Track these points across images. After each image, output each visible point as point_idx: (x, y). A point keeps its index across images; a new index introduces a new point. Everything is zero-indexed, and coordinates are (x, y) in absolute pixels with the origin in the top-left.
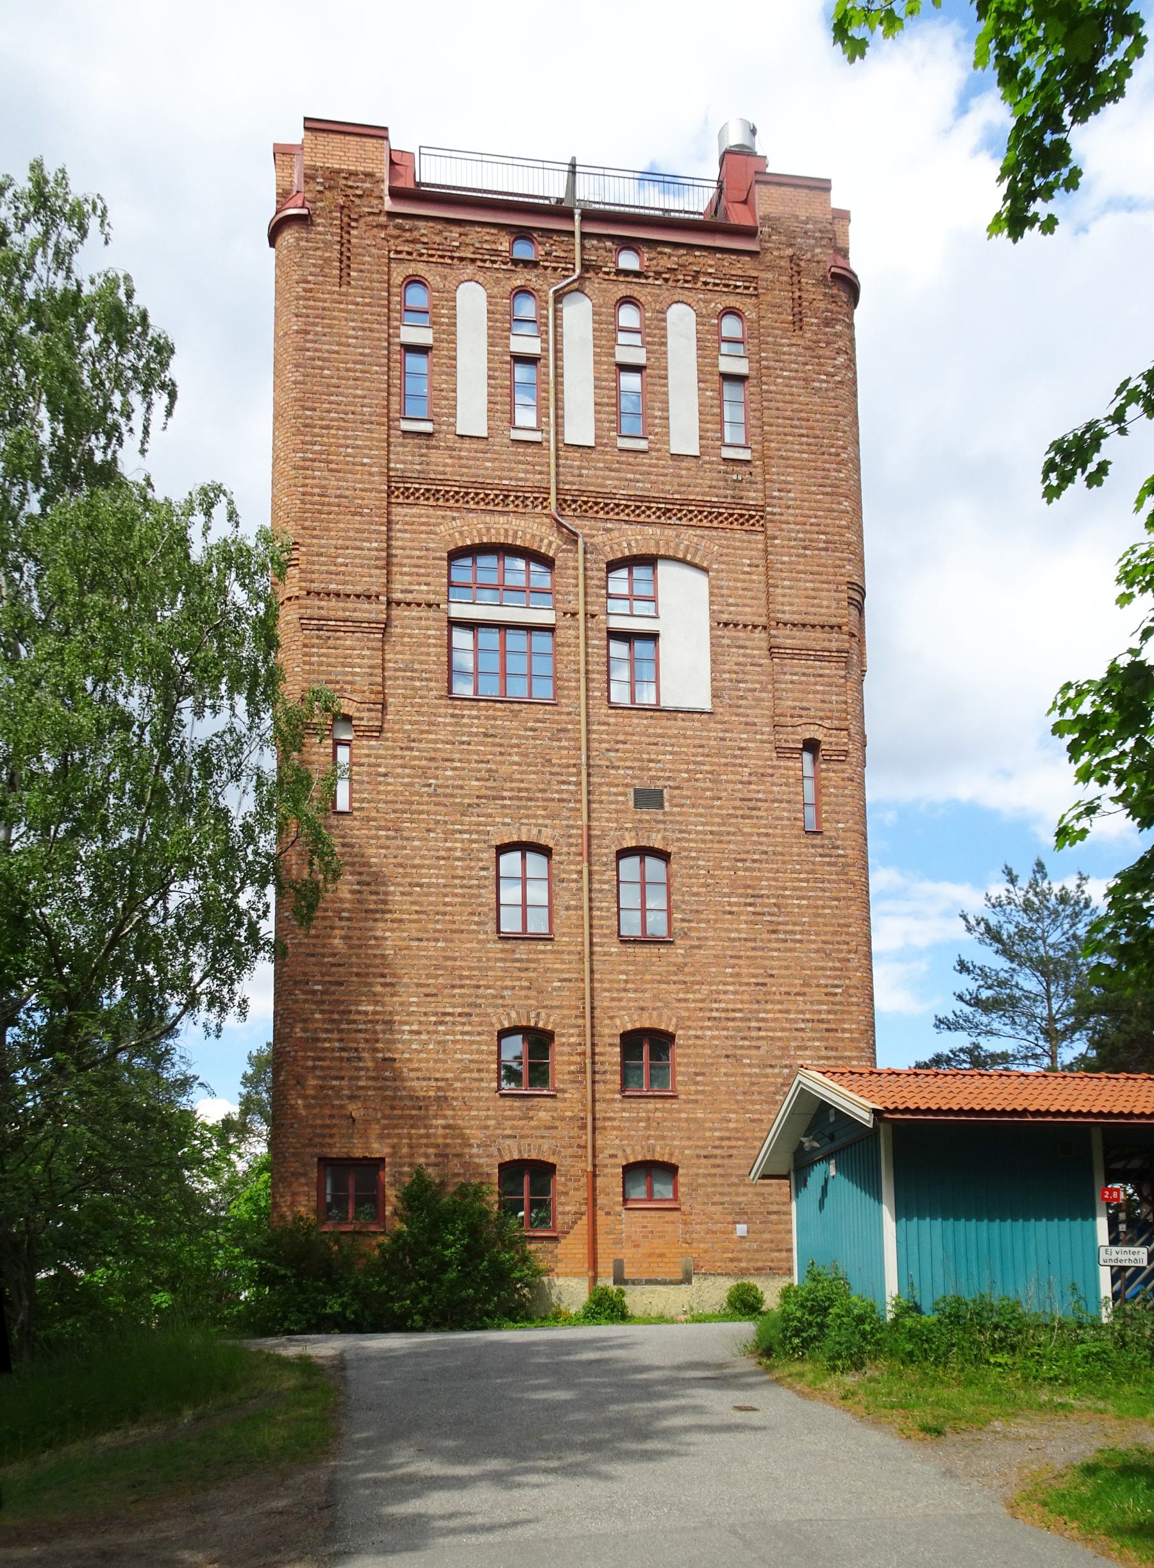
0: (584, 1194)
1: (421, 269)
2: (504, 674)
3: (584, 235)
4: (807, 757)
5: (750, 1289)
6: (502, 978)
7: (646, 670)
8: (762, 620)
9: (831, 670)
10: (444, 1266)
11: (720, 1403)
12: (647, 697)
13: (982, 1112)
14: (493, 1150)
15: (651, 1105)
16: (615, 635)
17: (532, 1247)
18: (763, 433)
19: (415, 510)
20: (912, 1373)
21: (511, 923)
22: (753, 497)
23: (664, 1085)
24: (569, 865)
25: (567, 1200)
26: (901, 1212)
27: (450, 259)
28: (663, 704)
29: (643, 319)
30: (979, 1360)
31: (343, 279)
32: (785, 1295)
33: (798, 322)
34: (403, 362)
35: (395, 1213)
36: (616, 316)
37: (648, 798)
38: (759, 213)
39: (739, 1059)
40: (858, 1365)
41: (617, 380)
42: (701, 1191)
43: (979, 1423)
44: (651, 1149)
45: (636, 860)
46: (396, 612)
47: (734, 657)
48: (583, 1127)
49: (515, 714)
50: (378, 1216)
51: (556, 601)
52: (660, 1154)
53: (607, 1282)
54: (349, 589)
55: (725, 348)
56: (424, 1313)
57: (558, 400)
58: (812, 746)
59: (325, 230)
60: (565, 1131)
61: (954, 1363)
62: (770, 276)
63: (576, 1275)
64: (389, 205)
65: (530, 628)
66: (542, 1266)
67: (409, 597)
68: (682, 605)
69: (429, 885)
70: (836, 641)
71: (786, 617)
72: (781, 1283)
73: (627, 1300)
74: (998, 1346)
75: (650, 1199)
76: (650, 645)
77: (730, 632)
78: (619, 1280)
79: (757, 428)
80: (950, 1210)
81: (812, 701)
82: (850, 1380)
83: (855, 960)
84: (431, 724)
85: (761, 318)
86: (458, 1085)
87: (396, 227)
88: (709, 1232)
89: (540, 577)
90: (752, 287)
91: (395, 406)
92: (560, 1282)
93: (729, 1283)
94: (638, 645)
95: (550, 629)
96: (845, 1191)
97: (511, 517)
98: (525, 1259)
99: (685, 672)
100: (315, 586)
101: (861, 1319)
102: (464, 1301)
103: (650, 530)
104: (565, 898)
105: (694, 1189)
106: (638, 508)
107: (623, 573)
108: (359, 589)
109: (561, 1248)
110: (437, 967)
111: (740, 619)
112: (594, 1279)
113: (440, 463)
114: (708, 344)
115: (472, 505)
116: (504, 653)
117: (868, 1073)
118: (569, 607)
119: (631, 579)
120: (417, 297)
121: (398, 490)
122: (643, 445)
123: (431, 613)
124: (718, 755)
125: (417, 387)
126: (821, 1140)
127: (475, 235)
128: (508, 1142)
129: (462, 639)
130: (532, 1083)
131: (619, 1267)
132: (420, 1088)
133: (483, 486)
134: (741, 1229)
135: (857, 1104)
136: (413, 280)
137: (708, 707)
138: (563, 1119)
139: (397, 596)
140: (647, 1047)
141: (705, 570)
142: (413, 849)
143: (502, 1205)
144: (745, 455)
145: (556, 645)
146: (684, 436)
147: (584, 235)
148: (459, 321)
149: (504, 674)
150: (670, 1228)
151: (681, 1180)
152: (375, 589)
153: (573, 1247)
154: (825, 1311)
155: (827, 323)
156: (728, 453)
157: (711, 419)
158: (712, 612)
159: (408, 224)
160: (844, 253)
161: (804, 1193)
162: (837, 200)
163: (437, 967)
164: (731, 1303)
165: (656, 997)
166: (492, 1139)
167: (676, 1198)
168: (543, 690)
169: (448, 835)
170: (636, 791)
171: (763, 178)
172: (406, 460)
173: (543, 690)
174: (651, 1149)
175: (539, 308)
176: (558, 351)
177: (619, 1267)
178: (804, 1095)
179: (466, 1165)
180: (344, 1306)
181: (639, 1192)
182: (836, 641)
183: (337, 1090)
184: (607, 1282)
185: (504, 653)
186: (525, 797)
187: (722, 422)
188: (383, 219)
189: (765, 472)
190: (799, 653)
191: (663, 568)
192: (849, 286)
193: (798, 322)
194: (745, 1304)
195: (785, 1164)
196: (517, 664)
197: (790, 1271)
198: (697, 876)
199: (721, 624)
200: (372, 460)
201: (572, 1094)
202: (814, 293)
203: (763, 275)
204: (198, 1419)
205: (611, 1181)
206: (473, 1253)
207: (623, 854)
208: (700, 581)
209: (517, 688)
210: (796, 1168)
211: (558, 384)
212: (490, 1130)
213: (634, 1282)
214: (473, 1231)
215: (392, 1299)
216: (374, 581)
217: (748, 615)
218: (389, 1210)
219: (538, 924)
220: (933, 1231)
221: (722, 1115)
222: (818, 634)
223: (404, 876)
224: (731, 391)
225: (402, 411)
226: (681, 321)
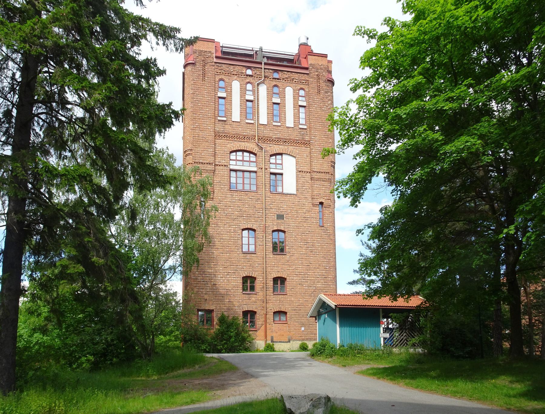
0: (263, 319)
1: (223, 77)
2: (243, 184)
3: (265, 69)
4: (320, 206)
5: (305, 344)
6: (243, 263)
7: (279, 183)
8: (309, 171)
9: (326, 184)
10: (231, 337)
11: (306, 363)
12: (280, 190)
13: (357, 305)
14: (241, 308)
15: (281, 296)
16: (271, 174)
17: (250, 333)
18: (310, 121)
19: (221, 141)
20: (342, 358)
21: (245, 249)
22: (307, 138)
23: (284, 292)
24: (259, 234)
25: (259, 320)
26: (341, 326)
27: (230, 74)
28: (285, 192)
29: (279, 91)
30: (355, 356)
31: (203, 80)
32: (314, 345)
33: (319, 92)
34: (218, 102)
35: (216, 324)
36: (272, 90)
37: (280, 217)
38: (309, 63)
39: (302, 285)
40: (331, 357)
41: (273, 107)
42: (293, 319)
43: (353, 365)
44: (280, 308)
45: (277, 233)
46: (217, 167)
47: (302, 180)
48: (264, 302)
49: (247, 195)
50: (212, 325)
51: (257, 165)
52: (283, 309)
53: (269, 342)
54: (205, 162)
55: (300, 98)
56: (225, 349)
57: (258, 112)
58: (321, 203)
59: (199, 66)
60: (259, 303)
61: (350, 355)
62: (312, 80)
63: (261, 340)
64: (215, 60)
65: (250, 172)
66: (254, 337)
67: (220, 164)
68: (288, 166)
69: (225, 239)
70: (328, 176)
71: (315, 170)
72: (314, 342)
73: (275, 346)
74: (358, 353)
75: (280, 321)
76: (281, 176)
77: (301, 173)
78: (272, 341)
79: (308, 118)
80: (351, 325)
81: (322, 192)
82: (330, 360)
83: (332, 259)
84: (225, 197)
85: (309, 91)
86: (232, 291)
87: (217, 66)
88: (295, 329)
89: (253, 158)
90: (307, 83)
91: (216, 113)
92: (257, 342)
93: (300, 342)
94: (278, 176)
95: (256, 172)
96: (329, 321)
97: (246, 143)
98: (249, 336)
99: (289, 184)
100: (196, 161)
101: (332, 348)
102: (235, 346)
103: (281, 146)
104: (259, 243)
105: (291, 318)
106: (278, 141)
107: (274, 157)
108: (207, 162)
109: (258, 333)
110: (227, 260)
111: (304, 170)
112: (266, 341)
113: (228, 128)
114: (296, 97)
115: (236, 139)
116: (243, 178)
117: (334, 294)
118: (260, 167)
119: (276, 159)
120: (222, 84)
121: (217, 135)
122: (279, 124)
123: (226, 168)
124: (298, 206)
125: (222, 108)
126: (323, 309)
127: (237, 68)
128: (245, 306)
129: (233, 174)
130: (250, 291)
131: (272, 338)
132: (222, 291)
133: (239, 134)
134: (303, 329)
135: (332, 303)
136: (221, 80)
137: (295, 193)
138: (258, 300)
139: (217, 163)
140: (279, 281)
141: (295, 157)
142: (221, 229)
143: (243, 322)
144: (305, 127)
145: (257, 176)
146: (290, 122)
147: (265, 69)
148: (233, 91)
149: (243, 184)
150: (285, 328)
151: (288, 316)
152: (211, 162)
153: (260, 333)
154: (325, 347)
155: (326, 92)
156: (301, 126)
157: (297, 116)
158: (297, 168)
159: (220, 65)
160: (330, 72)
161: (320, 321)
162: (329, 58)
163: (227, 260)
164: (300, 348)
165: (282, 269)
166: (241, 305)
167: (286, 321)
168: (254, 188)
169: (230, 226)
170: (277, 215)
171: (311, 53)
172: (219, 127)
173: (254, 188)
174: (280, 308)
175: (253, 87)
176: (258, 99)
177: (272, 338)
178: (320, 300)
179: (234, 312)
180: (206, 347)
181: (277, 319)
182: (328, 176)
183: (202, 292)
184: (269, 342)
185: (243, 178)
186: (249, 216)
187: (299, 118)
188: (213, 64)
189: (310, 132)
190: (319, 179)
191: (284, 156)
192: (332, 82)
193: (319, 92)
194: (304, 348)
195: (316, 314)
196: (247, 181)
197: (315, 339)
198: (292, 237)
199: (299, 171)
200: (210, 127)
201: (261, 294)
202: (323, 85)
203: (310, 80)
204: (200, 367)
205: (270, 316)
206: (238, 334)
207: (273, 231)
208: (293, 160)
209: (247, 187)
210: (318, 315)
211: (258, 108)
212: (239, 302)
213: (276, 342)
214: (237, 328)
215: (218, 346)
216: (211, 160)
217: (306, 169)
218: (215, 323)
219: (252, 248)
220: (347, 330)
221: (299, 299)
222: (323, 174)
223: (219, 236)
224: (302, 110)
225: (218, 114)
226: (289, 91)
